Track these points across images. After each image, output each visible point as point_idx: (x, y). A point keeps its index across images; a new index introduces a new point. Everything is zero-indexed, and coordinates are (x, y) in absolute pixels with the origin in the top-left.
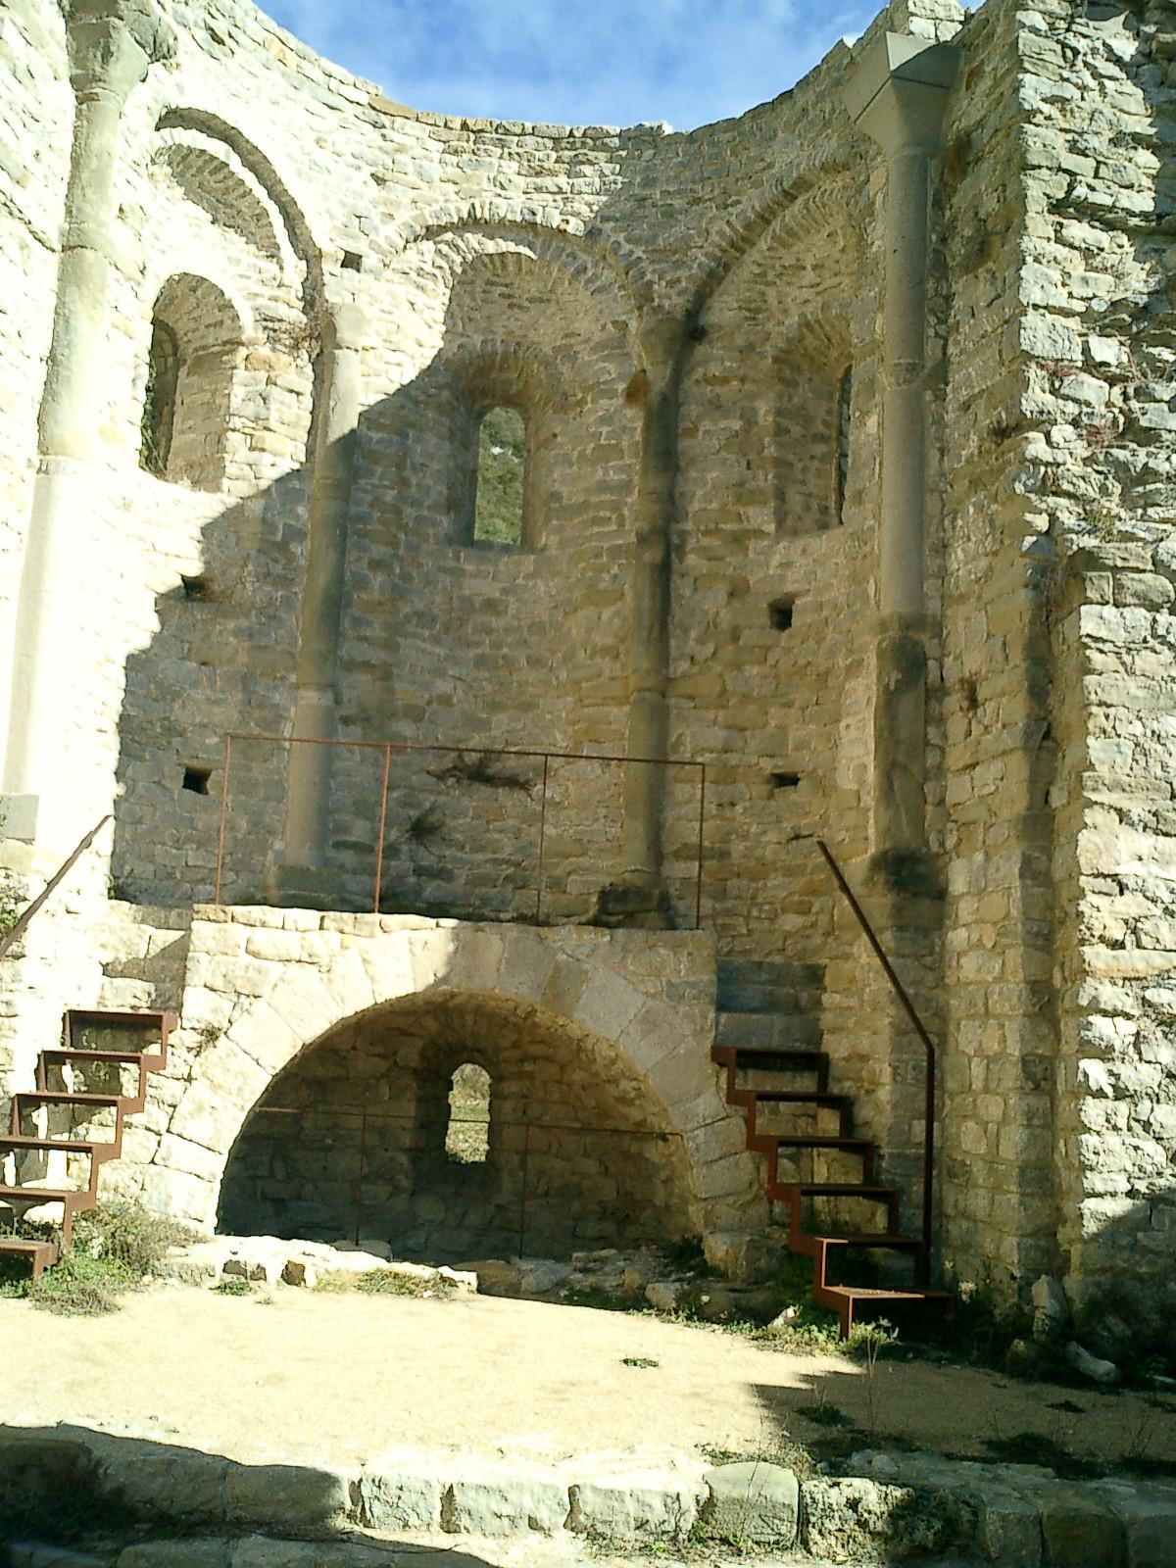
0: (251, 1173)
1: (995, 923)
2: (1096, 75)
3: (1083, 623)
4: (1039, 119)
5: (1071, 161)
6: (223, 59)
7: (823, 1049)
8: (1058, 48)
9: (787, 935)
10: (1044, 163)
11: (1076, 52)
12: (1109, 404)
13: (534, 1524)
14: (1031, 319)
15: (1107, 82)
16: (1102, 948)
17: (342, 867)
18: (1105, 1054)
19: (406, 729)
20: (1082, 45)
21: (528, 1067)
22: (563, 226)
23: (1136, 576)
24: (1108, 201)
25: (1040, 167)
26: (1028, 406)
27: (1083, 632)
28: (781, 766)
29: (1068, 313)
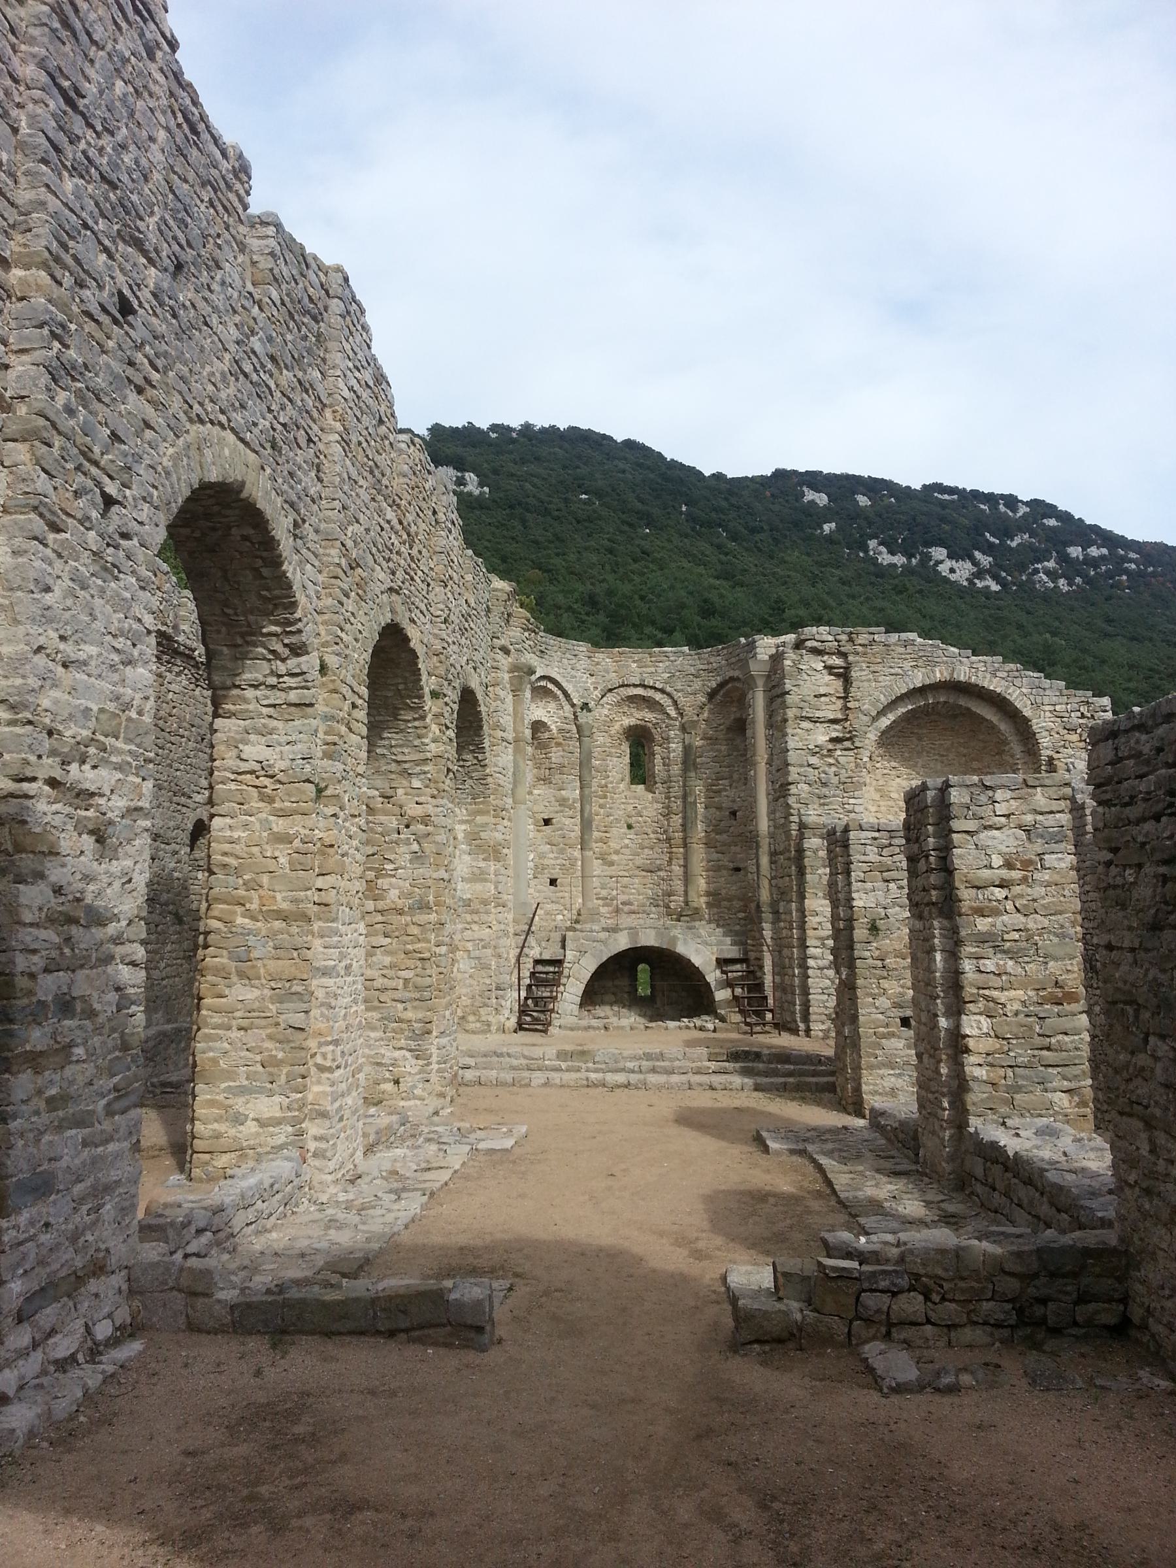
19: (615, 857)
20: (803, 667)
26: (790, 779)
28: (736, 865)
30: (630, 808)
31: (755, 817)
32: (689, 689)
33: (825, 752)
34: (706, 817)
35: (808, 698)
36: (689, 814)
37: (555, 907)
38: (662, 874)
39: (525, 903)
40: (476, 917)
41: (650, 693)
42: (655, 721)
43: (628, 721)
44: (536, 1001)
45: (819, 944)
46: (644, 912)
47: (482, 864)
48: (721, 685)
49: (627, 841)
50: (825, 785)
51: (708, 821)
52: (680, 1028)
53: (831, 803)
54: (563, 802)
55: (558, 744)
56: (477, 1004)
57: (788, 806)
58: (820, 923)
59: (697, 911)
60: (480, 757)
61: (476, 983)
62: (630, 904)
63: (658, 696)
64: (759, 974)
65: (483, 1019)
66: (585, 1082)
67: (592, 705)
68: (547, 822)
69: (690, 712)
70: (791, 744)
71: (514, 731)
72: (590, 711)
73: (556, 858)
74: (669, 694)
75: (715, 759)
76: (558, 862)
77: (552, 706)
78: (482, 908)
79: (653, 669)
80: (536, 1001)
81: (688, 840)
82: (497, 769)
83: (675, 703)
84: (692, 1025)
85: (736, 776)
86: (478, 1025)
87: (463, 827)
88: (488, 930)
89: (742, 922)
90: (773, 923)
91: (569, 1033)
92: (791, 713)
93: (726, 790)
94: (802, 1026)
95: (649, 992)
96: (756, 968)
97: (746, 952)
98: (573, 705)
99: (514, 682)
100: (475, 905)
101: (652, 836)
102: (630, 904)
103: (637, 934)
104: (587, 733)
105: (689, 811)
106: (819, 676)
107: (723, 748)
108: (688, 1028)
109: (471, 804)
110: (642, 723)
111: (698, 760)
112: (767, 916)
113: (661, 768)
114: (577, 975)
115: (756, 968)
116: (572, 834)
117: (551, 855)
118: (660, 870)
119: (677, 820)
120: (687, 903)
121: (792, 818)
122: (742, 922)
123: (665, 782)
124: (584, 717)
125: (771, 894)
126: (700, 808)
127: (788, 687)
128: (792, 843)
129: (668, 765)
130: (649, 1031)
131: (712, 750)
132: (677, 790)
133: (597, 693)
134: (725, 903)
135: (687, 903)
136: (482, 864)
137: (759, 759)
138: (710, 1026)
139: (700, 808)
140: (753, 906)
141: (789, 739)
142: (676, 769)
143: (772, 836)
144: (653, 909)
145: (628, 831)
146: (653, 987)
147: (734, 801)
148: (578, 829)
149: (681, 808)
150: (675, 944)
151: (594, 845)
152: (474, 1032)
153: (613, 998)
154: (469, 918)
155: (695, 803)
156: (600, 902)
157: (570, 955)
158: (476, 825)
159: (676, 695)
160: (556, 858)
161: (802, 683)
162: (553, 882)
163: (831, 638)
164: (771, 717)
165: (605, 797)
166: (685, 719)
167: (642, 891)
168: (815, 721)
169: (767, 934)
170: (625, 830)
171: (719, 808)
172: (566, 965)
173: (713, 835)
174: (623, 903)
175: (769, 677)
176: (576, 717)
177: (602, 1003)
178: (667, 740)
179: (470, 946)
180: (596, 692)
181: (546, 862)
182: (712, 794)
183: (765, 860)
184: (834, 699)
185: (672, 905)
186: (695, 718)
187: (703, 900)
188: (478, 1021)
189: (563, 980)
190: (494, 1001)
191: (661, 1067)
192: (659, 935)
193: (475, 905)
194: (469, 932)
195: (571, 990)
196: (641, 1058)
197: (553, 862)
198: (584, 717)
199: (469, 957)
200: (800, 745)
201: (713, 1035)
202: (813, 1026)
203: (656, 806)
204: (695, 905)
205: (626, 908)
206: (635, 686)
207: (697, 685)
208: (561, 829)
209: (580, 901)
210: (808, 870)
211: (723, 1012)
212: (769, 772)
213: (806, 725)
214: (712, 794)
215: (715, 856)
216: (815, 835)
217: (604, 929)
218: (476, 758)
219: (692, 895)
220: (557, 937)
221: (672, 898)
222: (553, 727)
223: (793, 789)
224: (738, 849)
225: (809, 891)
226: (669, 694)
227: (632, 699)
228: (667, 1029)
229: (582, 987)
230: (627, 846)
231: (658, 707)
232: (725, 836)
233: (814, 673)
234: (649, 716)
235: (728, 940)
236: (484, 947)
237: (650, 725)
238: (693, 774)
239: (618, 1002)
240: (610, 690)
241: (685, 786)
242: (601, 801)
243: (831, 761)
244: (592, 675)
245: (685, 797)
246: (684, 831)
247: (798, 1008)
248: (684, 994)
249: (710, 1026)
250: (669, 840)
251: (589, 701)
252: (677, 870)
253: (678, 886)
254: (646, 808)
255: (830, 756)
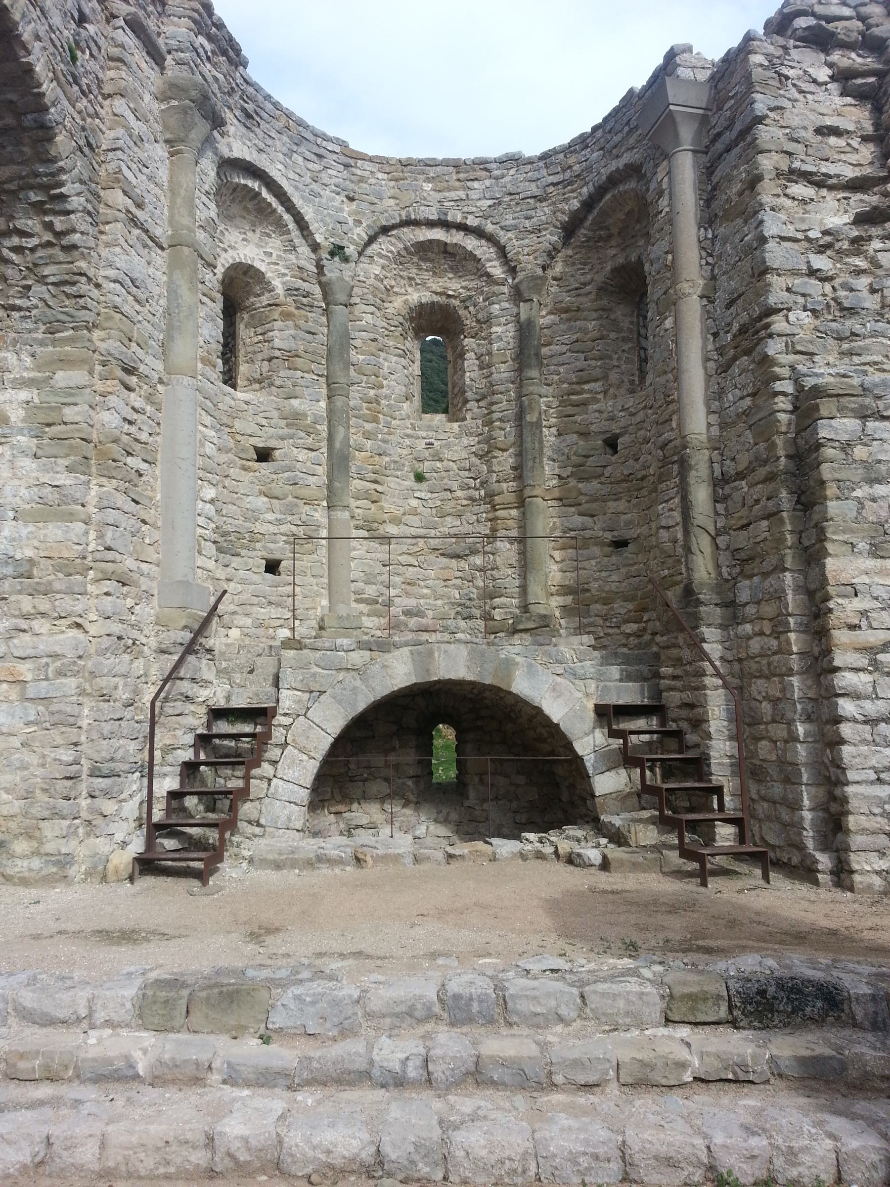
0: (321, 798)
1: (770, 620)
2: (801, 92)
3: (819, 431)
4: (767, 121)
5: (791, 147)
6: (254, 128)
7: (663, 702)
8: (776, 76)
9: (629, 635)
10: (773, 148)
11: (787, 78)
12: (824, 295)
13: (561, 1019)
14: (771, 245)
15: (808, 96)
16: (845, 631)
17: (361, 613)
18: (856, 696)
20: (791, 73)
21: (479, 723)
22: (464, 221)
23: (853, 399)
24: (814, 169)
25: (770, 151)
26: (772, 300)
27: (820, 436)
29: (796, 240)
30: (421, 445)
31: (678, 411)
32: (527, 223)
33: (845, 245)
34: (559, 451)
35: (803, 133)
36: (528, 445)
37: (275, 612)
38: (478, 560)
39: (186, 584)
40: (44, 605)
41: (456, 238)
42: (464, 293)
43: (416, 296)
44: (211, 799)
45: (862, 661)
46: (445, 629)
47: (65, 479)
48: (588, 205)
49: (414, 503)
50: (850, 311)
51: (563, 458)
52: (523, 856)
53: (866, 350)
54: (294, 419)
55: (287, 316)
56: (35, 811)
57: (766, 361)
58: (864, 613)
59: (544, 624)
60: (59, 223)
61: (34, 759)
62: (419, 614)
63: (471, 243)
64: (691, 738)
65: (50, 847)
66: (199, 1157)
67: (351, 250)
68: (264, 455)
69: (529, 264)
70: (772, 226)
71: (171, 222)
72: (346, 260)
73: (280, 523)
74: (491, 239)
75: (575, 347)
76: (284, 528)
77: (275, 244)
78: (59, 582)
79: (462, 194)
80: (211, 799)
81: (528, 492)
82: (111, 273)
83: (502, 252)
84: (548, 850)
85: (614, 376)
86: (36, 863)
87: (24, 395)
88: (75, 633)
89: (633, 641)
90: (723, 627)
91: (271, 876)
92: (767, 163)
93: (598, 401)
94: (824, 861)
95: (453, 773)
96: (684, 725)
97: (657, 693)
98: (315, 247)
99: (172, 121)
100: (43, 574)
101: (459, 493)
102: (419, 614)
103: (430, 654)
104: (341, 297)
105: (528, 438)
106: (821, 95)
107: (591, 325)
108: (540, 856)
109: (42, 343)
110: (442, 300)
111: (544, 351)
112: (711, 612)
113: (476, 374)
114: (302, 742)
115: (684, 725)
116: (312, 480)
117: (270, 516)
118: (474, 552)
119: (505, 461)
120: (525, 608)
121: (778, 386)
122: (633, 641)
123: (484, 397)
124: (334, 269)
125: (718, 566)
126: (549, 436)
127: (760, 107)
128: (779, 441)
129: (489, 366)
130: (455, 865)
131: (570, 329)
132: (504, 406)
133: (360, 233)
134: (596, 608)
135: (525, 608)
136: (65, 479)
137: (685, 287)
138: (593, 855)
139: (549, 436)
140: (673, 595)
141: (767, 216)
142: (503, 371)
143: (717, 445)
144: (462, 624)
145: (416, 486)
146: (461, 765)
147: (612, 419)
148: (321, 470)
149: (511, 439)
150: (509, 677)
151: (353, 503)
152: (24, 882)
153: (384, 788)
154: (27, 604)
155: (538, 425)
156: (363, 607)
157: (288, 700)
158: (54, 391)
159: (504, 237)
160: (280, 523)
161: (787, 104)
162: (272, 567)
163: (847, 12)
164: (708, 202)
165: (376, 420)
166: (521, 276)
167: (441, 591)
168: (819, 182)
169: (713, 648)
170: (410, 482)
171: (584, 435)
172: (280, 719)
173: (573, 482)
174: (408, 613)
175: (704, 120)
176: (320, 267)
177: (365, 797)
178: (488, 321)
179: (25, 670)
180: (358, 230)
181: (259, 527)
182: (570, 410)
183: (701, 495)
184: (855, 143)
185: (497, 614)
186: (539, 271)
187: (556, 602)
188: (36, 853)
189: (273, 753)
190: (84, 803)
191: (503, 1063)
192: (476, 657)
193: (43, 574)
194: (26, 637)
195: (289, 774)
196: (430, 1016)
197: (272, 529)
198: (334, 269)
199: (25, 699)
200: (789, 230)
201: (604, 880)
202: (857, 862)
203: (465, 441)
204: (541, 609)
205: (413, 622)
206: (431, 224)
207: (543, 213)
208: (290, 469)
209: (325, 602)
210: (831, 490)
211: (617, 821)
212: (708, 315)
213: (800, 190)
214: (570, 410)
215: (578, 520)
216: (841, 409)
217: (362, 646)
218: (49, 226)
219: (536, 592)
220: (267, 665)
221: (497, 601)
222: (277, 283)
223: (778, 324)
224: (622, 505)
225: (835, 537)
226: (491, 239)
227: (423, 249)
228: (493, 858)
229: (312, 767)
230: (414, 512)
231: (470, 265)
232: (595, 483)
233: (812, 87)
234: (455, 285)
235: (615, 671)
236: (60, 673)
237: (456, 302)
238: (534, 373)
239: (396, 794)
240: (385, 230)
241: (520, 396)
242: (368, 426)
243: (860, 262)
244: (351, 199)
245: (520, 416)
246: (519, 478)
247: (807, 815)
248: (521, 780)
249: (593, 855)
250: (491, 495)
251: (344, 243)
252: (507, 551)
253: (509, 579)
254: (448, 446)
255: (858, 253)
